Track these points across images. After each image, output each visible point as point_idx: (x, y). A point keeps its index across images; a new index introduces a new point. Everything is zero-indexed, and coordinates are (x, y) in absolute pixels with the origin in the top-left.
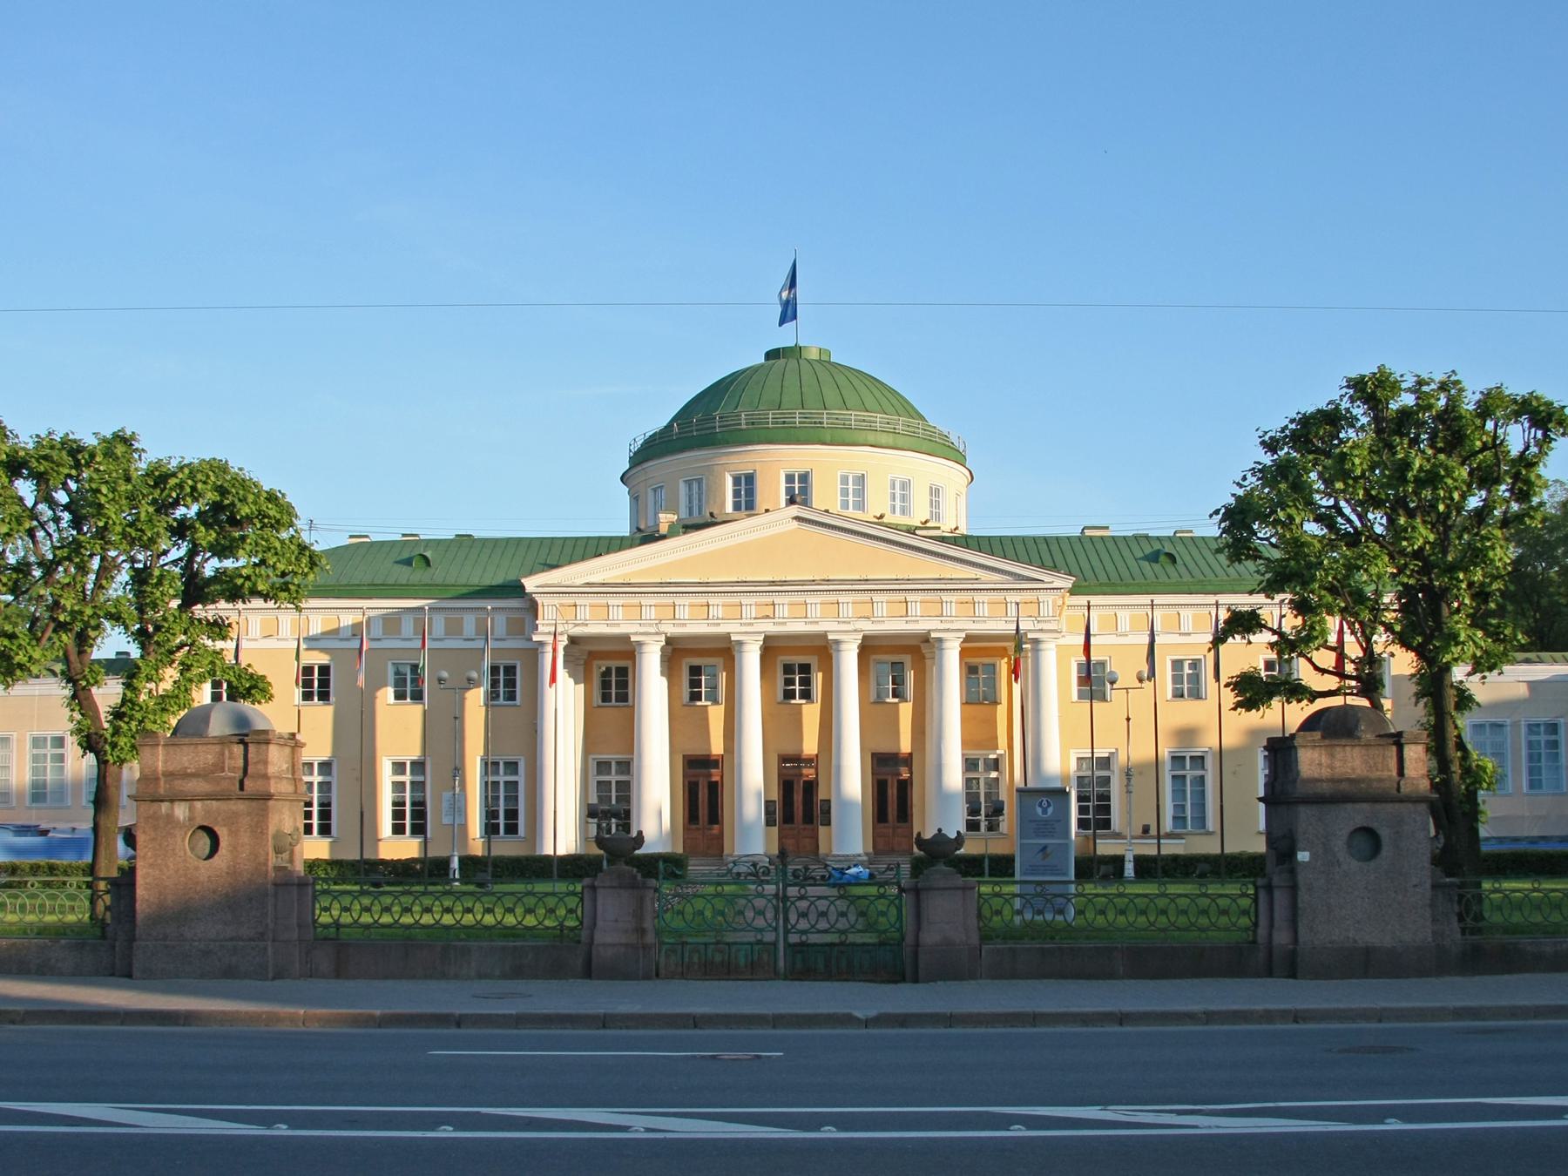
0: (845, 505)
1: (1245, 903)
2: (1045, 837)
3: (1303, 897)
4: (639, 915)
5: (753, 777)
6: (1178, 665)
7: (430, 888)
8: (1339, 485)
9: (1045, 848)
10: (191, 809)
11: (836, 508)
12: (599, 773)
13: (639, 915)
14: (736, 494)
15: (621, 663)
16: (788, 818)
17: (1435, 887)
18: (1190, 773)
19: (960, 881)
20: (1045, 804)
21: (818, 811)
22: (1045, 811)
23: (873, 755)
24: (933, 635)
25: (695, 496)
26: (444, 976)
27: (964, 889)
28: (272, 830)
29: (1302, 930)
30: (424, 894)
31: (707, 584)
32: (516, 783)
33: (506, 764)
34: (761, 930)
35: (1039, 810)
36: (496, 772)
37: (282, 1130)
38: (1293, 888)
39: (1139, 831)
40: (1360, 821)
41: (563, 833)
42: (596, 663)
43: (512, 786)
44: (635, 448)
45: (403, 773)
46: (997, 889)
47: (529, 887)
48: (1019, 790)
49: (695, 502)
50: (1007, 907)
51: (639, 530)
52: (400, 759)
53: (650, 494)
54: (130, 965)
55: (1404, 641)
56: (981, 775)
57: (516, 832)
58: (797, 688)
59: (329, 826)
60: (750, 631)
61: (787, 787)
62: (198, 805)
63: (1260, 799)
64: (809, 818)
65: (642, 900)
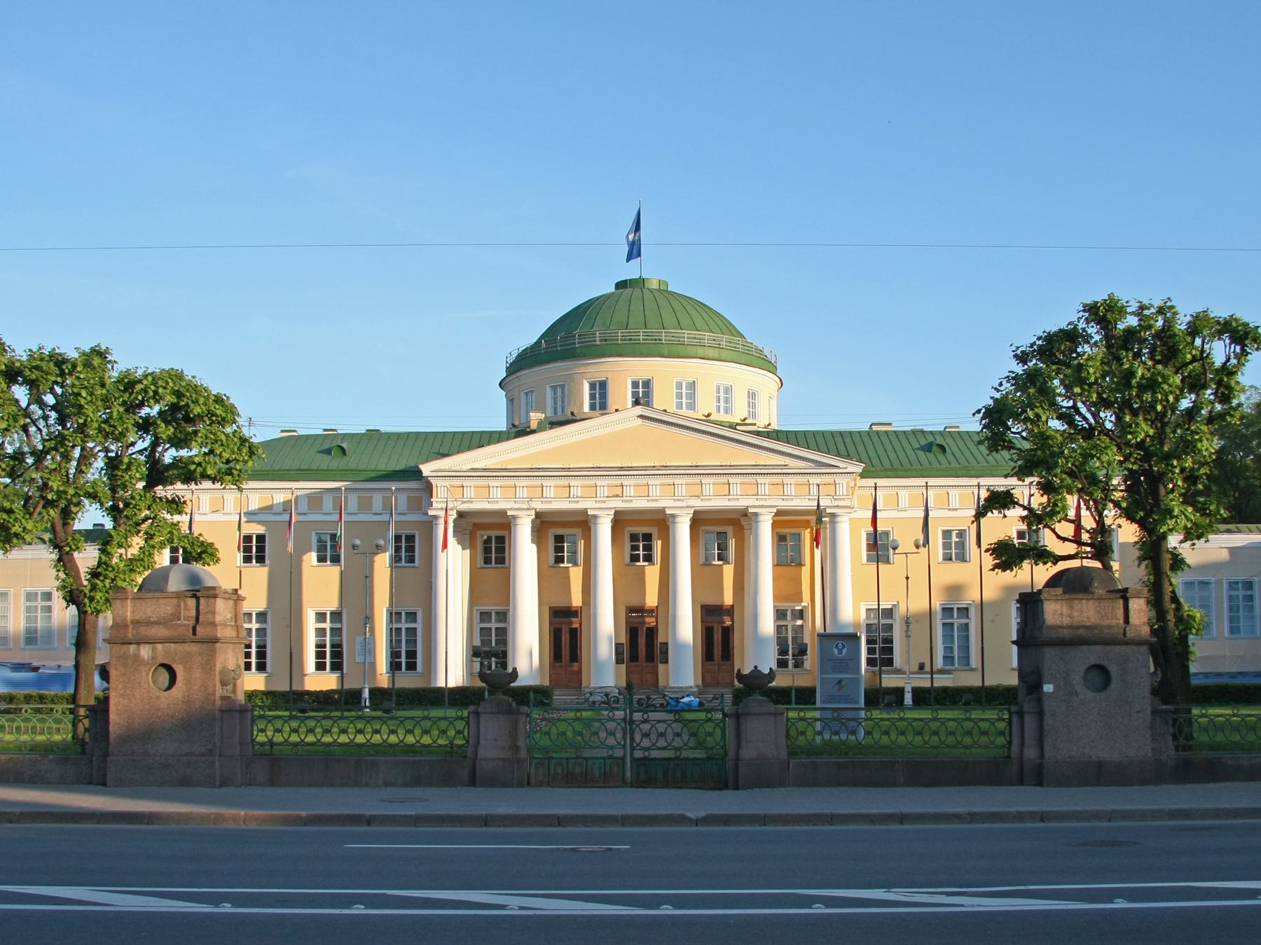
0: (680, 406)
1: (1001, 725)
2: (840, 672)
3: (1048, 721)
4: (514, 735)
5: (606, 625)
6: (947, 534)
7: (346, 714)
8: (1077, 390)
9: (840, 681)
10: (154, 650)
11: (672, 408)
12: (482, 621)
13: (514, 735)
14: (592, 397)
15: (500, 533)
16: (634, 657)
17: (1154, 712)
18: (957, 621)
19: (772, 708)
20: (840, 646)
21: (657, 651)
22: (840, 652)
23: (702, 606)
24: (751, 510)
25: (559, 399)
26: (357, 784)
27: (775, 714)
28: (218, 667)
29: (1047, 747)
30: (341, 718)
31: (569, 469)
32: (415, 629)
33: (407, 614)
34: (612, 748)
35: (836, 651)
36: (399, 621)
37: (227, 908)
38: (1040, 714)
39: (916, 668)
40: (1093, 660)
41: (453, 670)
42: (479, 533)
43: (412, 632)
44: (511, 360)
45: (324, 621)
46: (802, 714)
47: (426, 713)
48: (819, 635)
49: (559, 404)
50: (810, 729)
51: (514, 426)
52: (322, 610)
53: (523, 397)
54: (105, 775)
55: (1129, 515)
56: (789, 622)
57: (415, 669)
58: (641, 553)
59: (264, 664)
60: (603, 507)
61: (633, 632)
62: (159, 647)
63: (1014, 642)
64: (650, 657)
65: (516, 723)
